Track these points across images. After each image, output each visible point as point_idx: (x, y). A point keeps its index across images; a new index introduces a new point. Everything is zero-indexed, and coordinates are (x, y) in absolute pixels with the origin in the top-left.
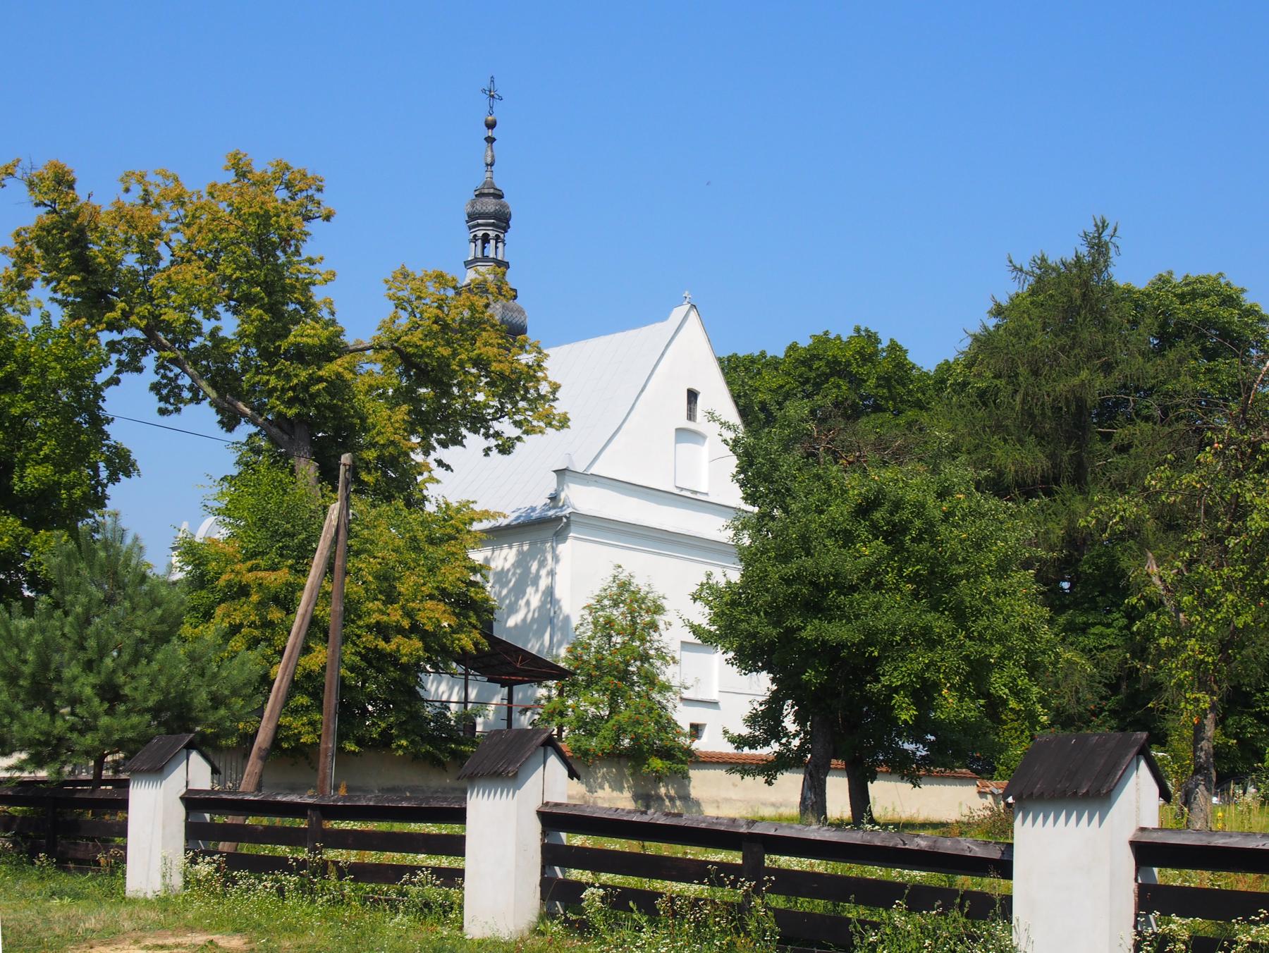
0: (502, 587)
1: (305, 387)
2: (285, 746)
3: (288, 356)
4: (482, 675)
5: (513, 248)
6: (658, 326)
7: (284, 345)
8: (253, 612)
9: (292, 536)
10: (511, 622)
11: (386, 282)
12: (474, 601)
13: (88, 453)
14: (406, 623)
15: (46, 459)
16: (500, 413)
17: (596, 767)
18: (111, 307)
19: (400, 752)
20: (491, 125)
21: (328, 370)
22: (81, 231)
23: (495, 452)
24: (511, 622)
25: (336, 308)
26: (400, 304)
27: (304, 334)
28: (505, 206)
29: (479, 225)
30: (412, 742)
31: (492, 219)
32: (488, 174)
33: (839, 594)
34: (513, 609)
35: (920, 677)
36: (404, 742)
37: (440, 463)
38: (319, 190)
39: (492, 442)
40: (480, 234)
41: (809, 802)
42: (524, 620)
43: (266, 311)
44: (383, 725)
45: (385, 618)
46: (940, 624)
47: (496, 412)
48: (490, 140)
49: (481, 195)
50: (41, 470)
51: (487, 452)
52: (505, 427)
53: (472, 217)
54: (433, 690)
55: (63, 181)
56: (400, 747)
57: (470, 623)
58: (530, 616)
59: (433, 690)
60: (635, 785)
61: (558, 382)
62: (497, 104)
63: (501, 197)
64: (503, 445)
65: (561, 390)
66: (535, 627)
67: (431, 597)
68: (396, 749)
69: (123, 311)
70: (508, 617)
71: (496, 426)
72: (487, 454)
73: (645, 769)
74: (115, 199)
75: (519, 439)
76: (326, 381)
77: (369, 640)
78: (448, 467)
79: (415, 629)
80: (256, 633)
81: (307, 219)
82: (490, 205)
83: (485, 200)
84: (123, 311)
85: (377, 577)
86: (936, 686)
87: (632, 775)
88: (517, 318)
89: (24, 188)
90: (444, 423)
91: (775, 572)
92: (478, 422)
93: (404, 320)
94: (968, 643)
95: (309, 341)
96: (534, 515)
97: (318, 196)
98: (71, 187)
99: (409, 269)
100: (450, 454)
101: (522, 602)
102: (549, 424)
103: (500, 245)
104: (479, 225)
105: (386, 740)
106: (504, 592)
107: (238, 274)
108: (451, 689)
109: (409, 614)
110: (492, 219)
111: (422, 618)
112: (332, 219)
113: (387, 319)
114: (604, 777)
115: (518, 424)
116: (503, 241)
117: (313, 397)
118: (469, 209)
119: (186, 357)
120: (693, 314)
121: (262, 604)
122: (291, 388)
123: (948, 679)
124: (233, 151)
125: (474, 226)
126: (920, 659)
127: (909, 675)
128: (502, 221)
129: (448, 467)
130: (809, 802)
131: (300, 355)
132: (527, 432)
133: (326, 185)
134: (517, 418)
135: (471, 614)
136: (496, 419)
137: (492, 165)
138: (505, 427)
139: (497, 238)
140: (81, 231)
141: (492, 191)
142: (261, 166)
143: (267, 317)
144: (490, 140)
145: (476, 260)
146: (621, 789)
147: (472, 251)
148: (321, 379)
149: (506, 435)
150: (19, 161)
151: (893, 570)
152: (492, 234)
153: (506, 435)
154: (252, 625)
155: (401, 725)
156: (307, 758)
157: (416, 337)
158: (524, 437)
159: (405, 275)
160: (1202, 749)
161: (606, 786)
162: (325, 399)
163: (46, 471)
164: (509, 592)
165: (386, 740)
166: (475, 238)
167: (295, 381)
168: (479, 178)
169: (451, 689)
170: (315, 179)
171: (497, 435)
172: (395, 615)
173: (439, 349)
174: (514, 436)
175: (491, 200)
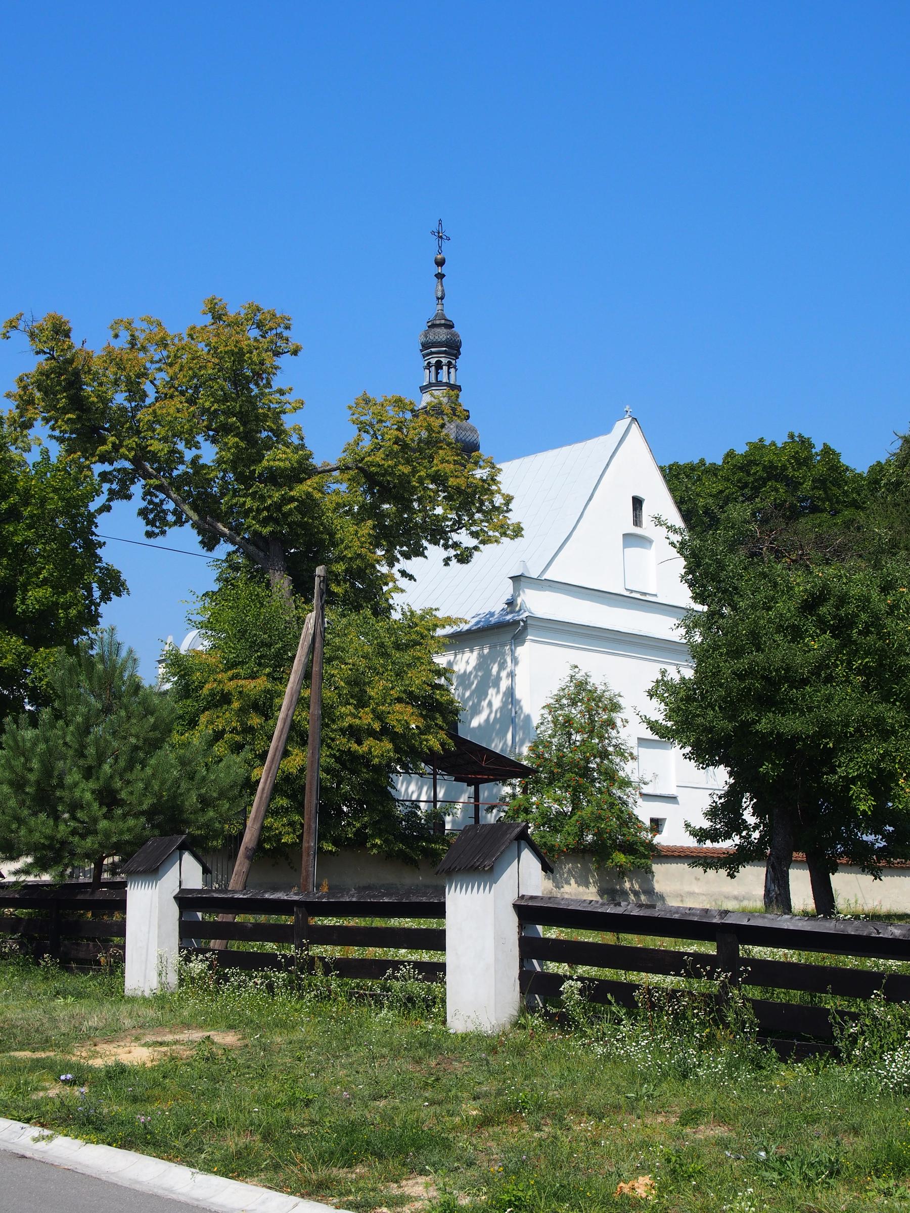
0: (465, 689)
1: (278, 506)
5: (464, 371)
7: (258, 469)
9: (269, 646)
10: (475, 723)
11: (350, 408)
14: (377, 726)
15: (45, 581)
16: (458, 525)
17: (561, 862)
18: (103, 441)
19: (375, 851)
20: (440, 263)
23: (454, 562)
24: (475, 723)
25: (304, 433)
26: (363, 428)
27: (277, 458)
28: (456, 335)
29: (432, 353)
32: (439, 307)
34: (476, 711)
36: (378, 841)
38: (287, 328)
39: (452, 552)
40: (433, 361)
44: (358, 825)
45: (357, 721)
47: (454, 524)
48: (440, 276)
49: (433, 326)
51: (447, 562)
52: (463, 538)
53: (425, 346)
55: (60, 331)
56: (374, 846)
57: (436, 725)
58: (493, 716)
60: (601, 879)
61: (511, 494)
62: (445, 244)
63: (452, 326)
65: (513, 501)
66: (498, 726)
69: (114, 444)
70: (472, 718)
71: (455, 537)
72: (447, 564)
73: (609, 863)
74: (106, 345)
75: (476, 548)
76: (297, 500)
77: (342, 742)
81: (277, 354)
82: (442, 334)
84: (114, 444)
88: (470, 437)
89: (26, 338)
91: (728, 668)
92: (438, 534)
93: (367, 442)
95: (281, 464)
96: (493, 620)
97: (286, 333)
99: (370, 395)
102: (504, 534)
103: (452, 370)
104: (432, 353)
106: (467, 694)
107: (216, 406)
109: (379, 717)
111: (392, 720)
112: (299, 354)
115: (474, 535)
116: (455, 367)
118: (423, 340)
120: (635, 427)
122: (266, 509)
125: (428, 354)
126: (874, 750)
127: (865, 766)
128: (453, 348)
131: (274, 478)
132: (483, 542)
134: (474, 529)
137: (442, 298)
138: (463, 538)
139: (449, 364)
141: (443, 322)
142: (235, 309)
144: (440, 276)
145: (430, 385)
146: (587, 885)
148: (292, 499)
149: (464, 546)
152: (444, 361)
153: (464, 546)
154: (234, 730)
157: (379, 457)
158: (481, 546)
159: (367, 401)
161: (572, 881)
162: (297, 517)
168: (431, 311)
171: (456, 545)
172: (366, 719)
173: (400, 467)
174: (471, 546)
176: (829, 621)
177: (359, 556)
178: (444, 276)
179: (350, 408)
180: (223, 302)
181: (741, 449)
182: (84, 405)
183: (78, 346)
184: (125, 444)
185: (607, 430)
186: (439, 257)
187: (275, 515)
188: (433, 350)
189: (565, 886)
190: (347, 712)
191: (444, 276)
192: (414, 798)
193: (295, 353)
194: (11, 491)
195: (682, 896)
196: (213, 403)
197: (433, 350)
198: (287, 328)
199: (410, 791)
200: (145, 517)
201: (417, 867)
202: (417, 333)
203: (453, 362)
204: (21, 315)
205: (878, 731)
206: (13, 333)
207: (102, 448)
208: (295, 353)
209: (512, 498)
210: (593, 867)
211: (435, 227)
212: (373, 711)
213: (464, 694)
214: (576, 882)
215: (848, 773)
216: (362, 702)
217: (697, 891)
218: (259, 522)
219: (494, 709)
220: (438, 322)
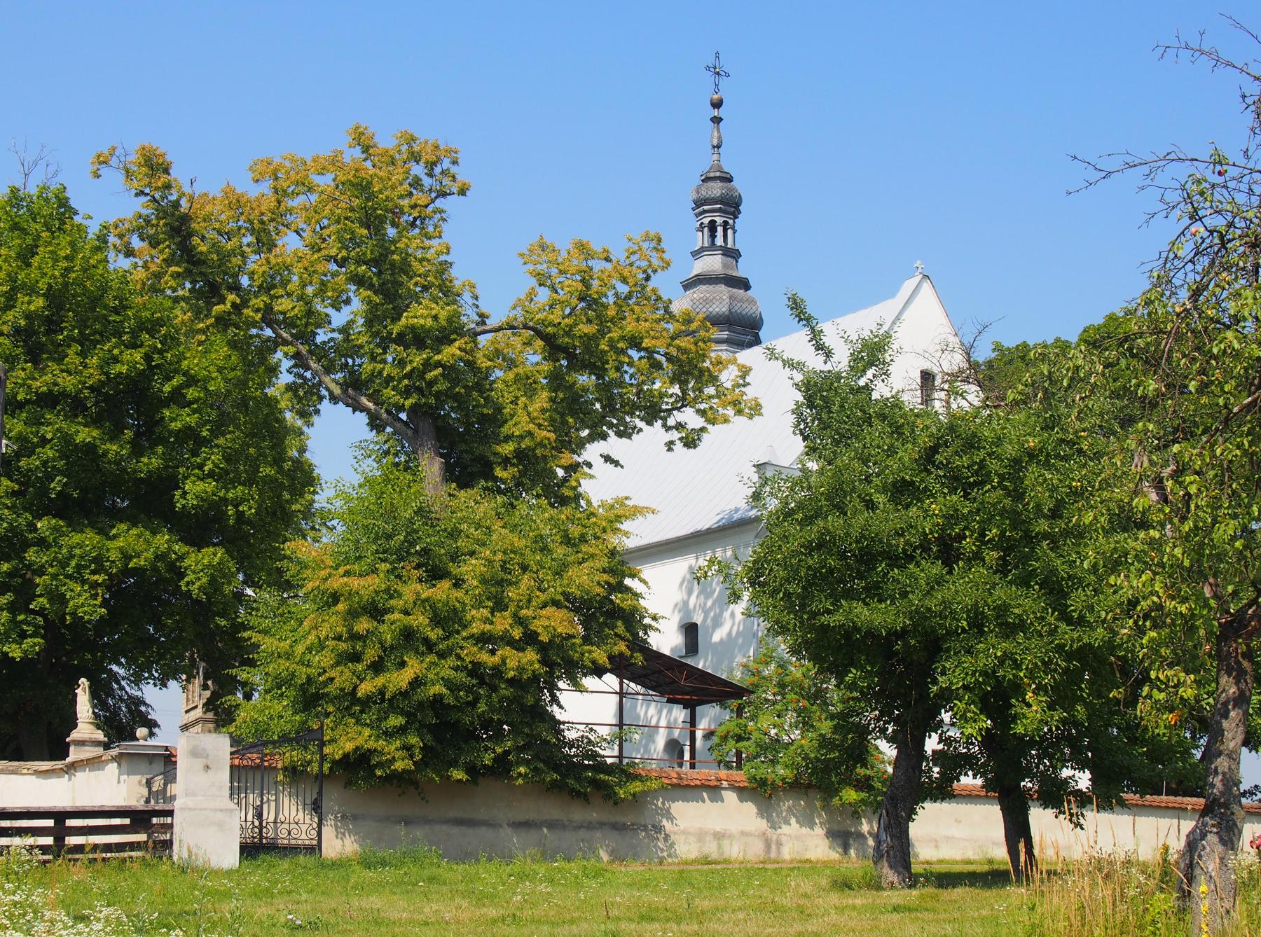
0: (707, 597)
1: (420, 373)
2: (379, 773)
3: (400, 339)
4: (662, 695)
5: (745, 234)
6: (889, 302)
7: (396, 329)
8: (341, 623)
9: (389, 537)
10: (716, 637)
11: (522, 255)
12: (621, 610)
13: (258, 467)
14: (517, 633)
15: (211, 475)
16: (682, 402)
17: (780, 800)
18: (222, 300)
19: (520, 781)
20: (717, 105)
21: (450, 353)
22: (186, 219)
23: (679, 446)
24: (716, 637)
25: (478, 291)
26: (542, 279)
27: (419, 315)
28: (734, 189)
29: (705, 212)
30: (536, 770)
31: (721, 206)
32: (715, 157)
33: (891, 566)
34: (717, 623)
35: (989, 674)
36: (522, 770)
37: (607, 459)
38: (455, 162)
39: (675, 435)
40: (706, 221)
41: (884, 847)
42: (730, 633)
43: (376, 293)
44: (499, 750)
45: (488, 627)
46: (1027, 603)
47: (676, 401)
48: (717, 120)
49: (707, 180)
50: (201, 486)
51: (670, 445)
52: (689, 417)
53: (698, 203)
54: (642, 714)
55: (155, 166)
56: (520, 774)
57: (616, 635)
58: (735, 629)
59: (642, 714)
60: (829, 821)
61: (748, 364)
62: (723, 82)
63: (730, 180)
64: (687, 437)
65: (752, 373)
66: (740, 641)
67: (556, 603)
68: (517, 778)
69: (234, 305)
70: (713, 631)
71: (678, 417)
72: (670, 449)
73: (836, 800)
74: (224, 185)
75: (703, 429)
76: (442, 366)
77: (472, 653)
78: (617, 463)
79: (530, 638)
80: (343, 646)
81: (443, 194)
82: (716, 189)
83: (711, 184)
84: (234, 305)
85: (483, 581)
86: (1017, 689)
87: (823, 808)
88: (747, 310)
89: (121, 176)
90: (617, 411)
91: (799, 536)
92: (653, 412)
93: (544, 295)
94: (1063, 626)
95: (422, 321)
96: (736, 517)
97: (454, 169)
98: (166, 171)
99: (548, 240)
100: (613, 445)
101: (727, 614)
102: (739, 412)
103: (730, 232)
104: (705, 212)
105: (502, 767)
106: (709, 603)
107: (344, 253)
108: (660, 712)
109: (519, 621)
110: (721, 206)
111: (536, 626)
112: (468, 193)
113: (523, 297)
114: (790, 810)
115: (702, 413)
116: (733, 228)
117: (431, 384)
118: (694, 196)
119: (310, 352)
120: (926, 286)
121: (353, 614)
122: (405, 377)
123: (1032, 678)
124: (353, 124)
125: (701, 214)
126: (992, 649)
127: (973, 674)
128: (731, 206)
129: (617, 463)
130: (884, 847)
131: (416, 338)
132: (713, 422)
133: (462, 158)
134: (702, 406)
135: (619, 623)
136: (678, 409)
137: (718, 147)
138: (689, 417)
139: (725, 224)
140: (186, 219)
141: (718, 174)
142: (386, 141)
143: (377, 299)
144: (717, 120)
145: (703, 249)
146: (811, 825)
147: (701, 239)
148: (438, 364)
149: (690, 427)
150: (114, 149)
151: (972, 533)
152: (719, 220)
153: (690, 427)
154: (339, 638)
155: (521, 749)
156: (417, 788)
157: (555, 317)
158: (710, 427)
159: (543, 248)
160: (1216, 772)
161: (793, 821)
162: (442, 386)
163: (210, 486)
164: (714, 604)
165: (502, 767)
166: (701, 228)
167: (408, 368)
168: (705, 162)
169: (660, 712)
170: (449, 151)
171: (679, 426)
172: (502, 623)
173: (581, 326)
174: (698, 427)
175: (719, 184)
176: (968, 478)
177: (530, 433)
178: (721, 119)
179: (522, 255)
180: (370, 131)
181: (1099, 320)
182: (193, 256)
183: (187, 189)
184: (251, 303)
185: (892, 294)
186: (716, 97)
187: (417, 382)
188: (706, 208)
189: (784, 826)
190: (479, 616)
191: (721, 119)
192: (653, 723)
193: (462, 192)
194: (176, 371)
195: (936, 841)
196: (340, 249)
197: (706, 208)
198: (455, 162)
199: (649, 715)
200: (296, 395)
201: (588, 801)
202: (689, 189)
203: (731, 222)
204: (114, 149)
205: (1000, 625)
206: (104, 171)
207: (218, 309)
208: (462, 192)
209: (751, 369)
210: (818, 804)
211: (710, 61)
212: (515, 615)
213: (705, 604)
214: (798, 822)
215: (951, 683)
216: (500, 605)
217: (957, 834)
218: (401, 393)
219: (737, 621)
220: (712, 175)
